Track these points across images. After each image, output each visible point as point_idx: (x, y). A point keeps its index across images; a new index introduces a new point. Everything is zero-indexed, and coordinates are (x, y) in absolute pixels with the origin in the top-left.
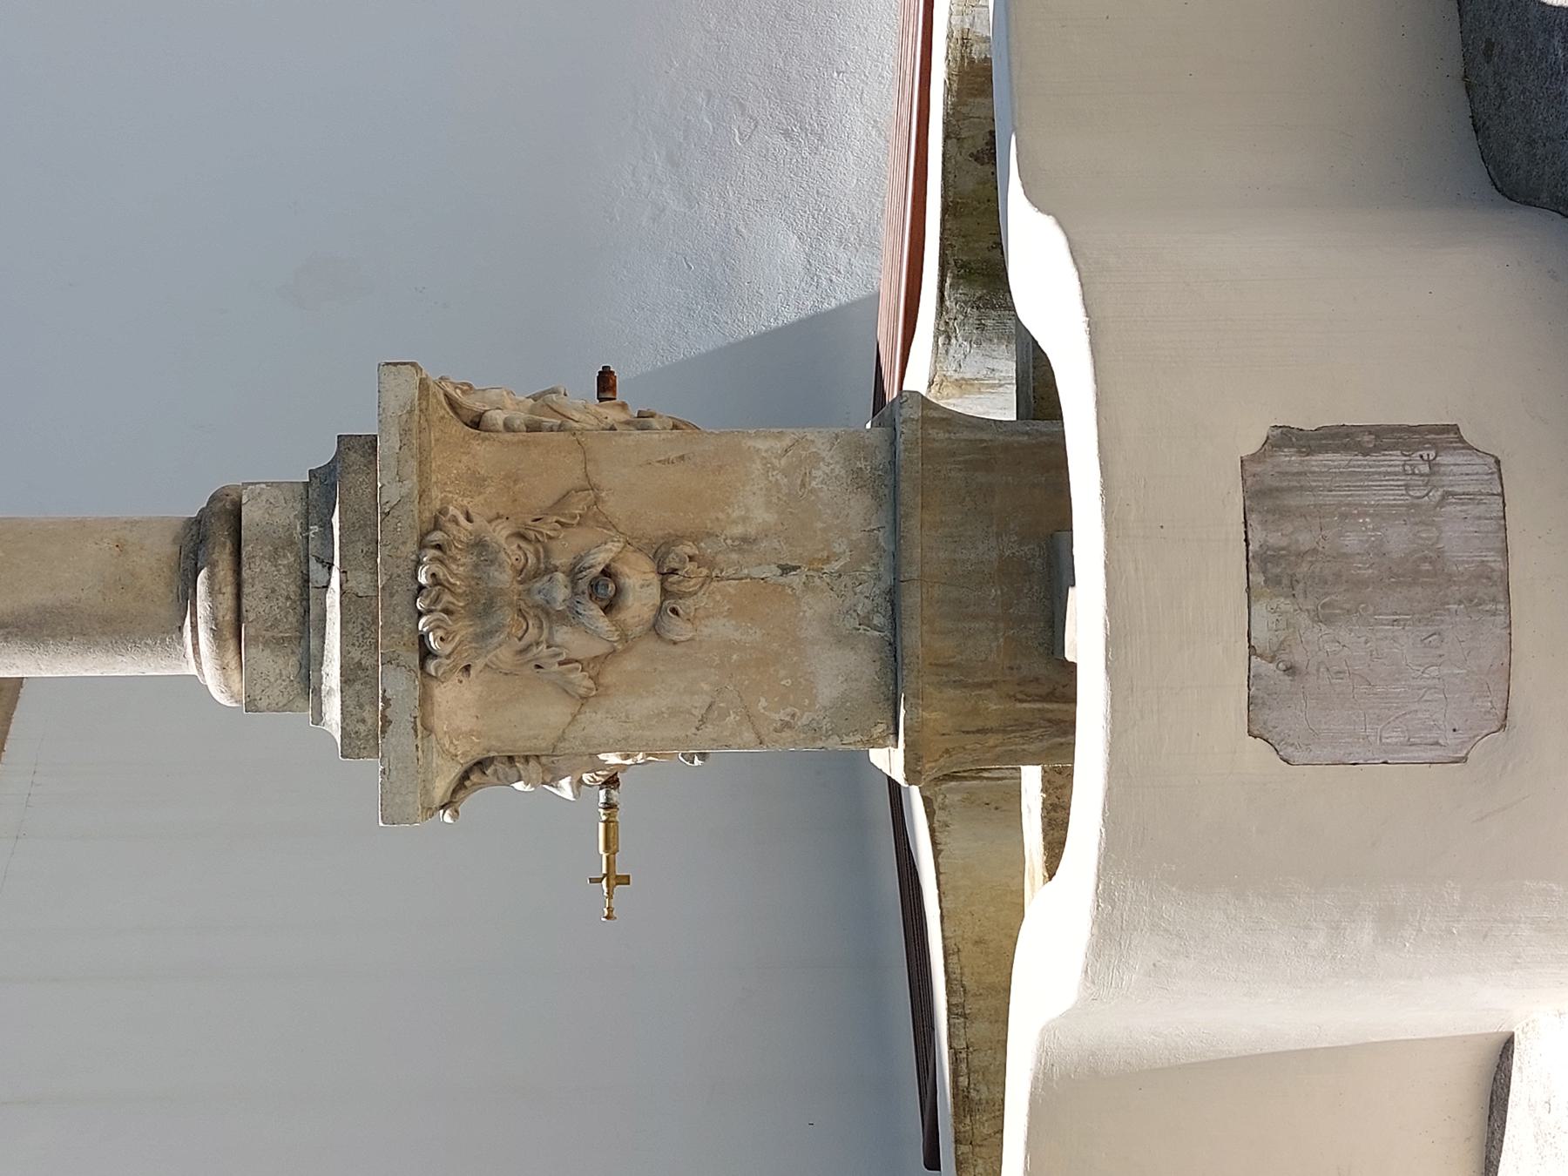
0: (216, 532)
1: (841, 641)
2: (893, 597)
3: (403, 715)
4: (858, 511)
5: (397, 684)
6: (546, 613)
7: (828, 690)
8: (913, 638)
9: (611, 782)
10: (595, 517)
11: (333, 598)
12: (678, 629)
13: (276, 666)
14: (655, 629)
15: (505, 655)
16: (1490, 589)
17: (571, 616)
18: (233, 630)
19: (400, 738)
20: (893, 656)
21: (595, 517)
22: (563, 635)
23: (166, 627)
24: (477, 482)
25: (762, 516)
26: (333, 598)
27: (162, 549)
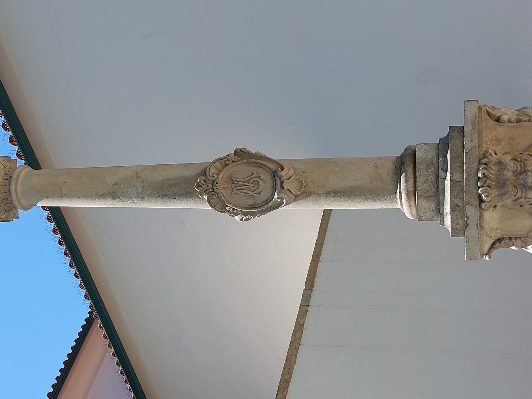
0: (407, 160)
5: (471, 211)
11: (448, 182)
13: (428, 205)
18: (413, 194)
19: (472, 230)
23: (390, 192)
24: (499, 141)
26: (448, 182)
27: (390, 166)
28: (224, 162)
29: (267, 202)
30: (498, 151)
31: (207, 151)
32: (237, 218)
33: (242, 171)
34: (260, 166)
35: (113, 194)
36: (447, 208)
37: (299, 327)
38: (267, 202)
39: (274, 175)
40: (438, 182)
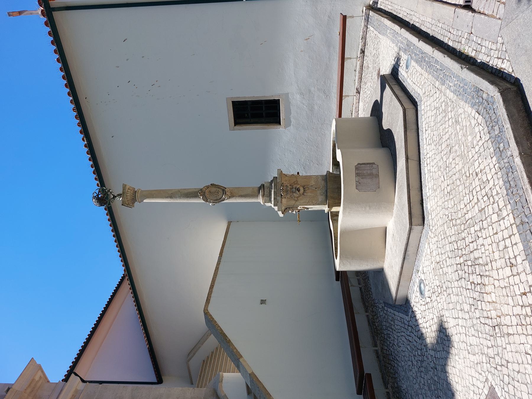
0: (262, 186)
1: (322, 195)
2: (326, 191)
3: (279, 202)
4: (323, 182)
5: (279, 198)
6: (293, 192)
7: (320, 200)
8: (328, 194)
9: (299, 211)
10: (297, 184)
11: (273, 192)
12: (305, 194)
13: (268, 199)
14: (303, 194)
15: (289, 196)
16: (377, 176)
17: (295, 192)
18: (263, 196)
19: (279, 203)
20: (326, 197)
21: (297, 184)
22: (294, 194)
23: (256, 196)
24: (286, 181)
25: (313, 183)
26: (273, 192)
27: (257, 189)
28: (208, 187)
29: (221, 198)
30: (286, 183)
31: (201, 185)
32: (211, 204)
33: (213, 189)
34: (219, 188)
35: (171, 197)
36: (273, 199)
37: (217, 269)
38: (221, 198)
39: (223, 190)
40: (270, 192)
